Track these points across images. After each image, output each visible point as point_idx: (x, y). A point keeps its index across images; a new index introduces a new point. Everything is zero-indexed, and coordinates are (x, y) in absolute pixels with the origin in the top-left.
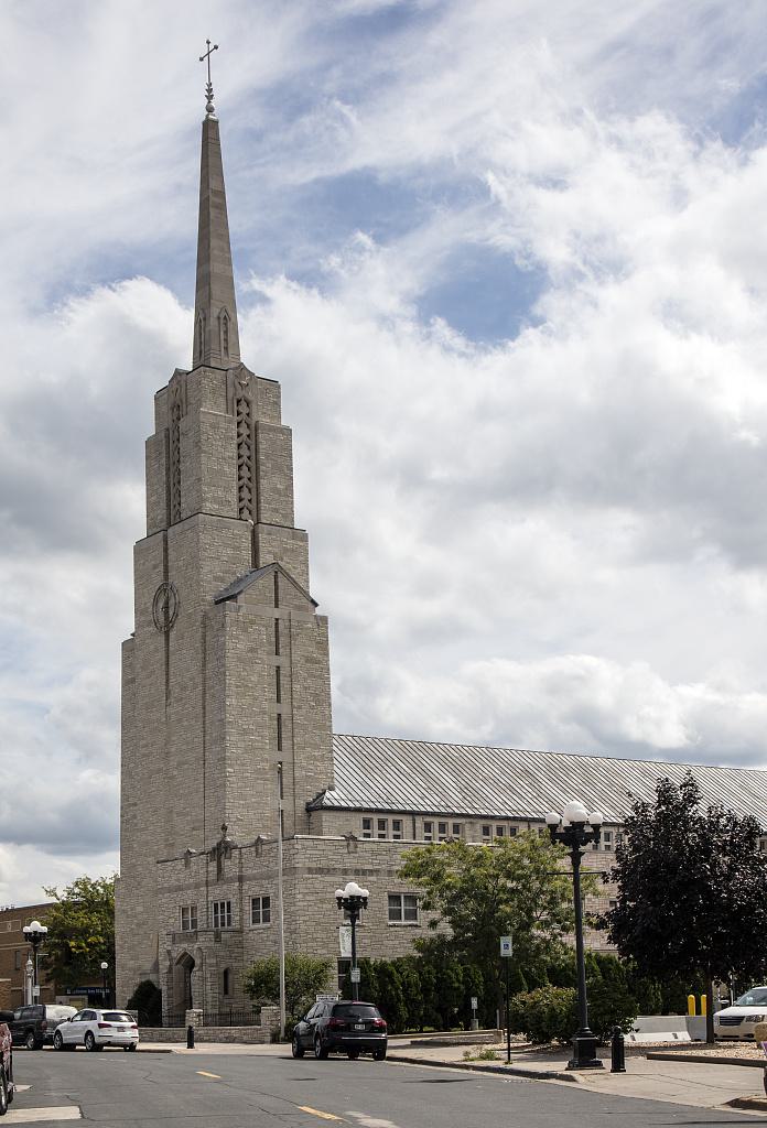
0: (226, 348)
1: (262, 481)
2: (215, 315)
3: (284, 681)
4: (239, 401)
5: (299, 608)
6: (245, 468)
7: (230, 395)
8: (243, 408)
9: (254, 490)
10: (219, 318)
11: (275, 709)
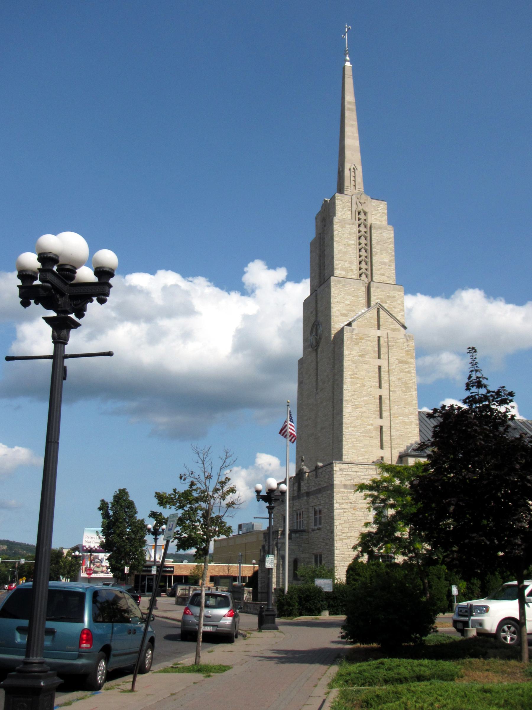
0: (355, 185)
1: (373, 257)
2: (348, 168)
3: (384, 375)
4: (359, 213)
5: (394, 330)
6: (363, 250)
7: (354, 209)
8: (362, 216)
9: (369, 263)
10: (350, 169)
11: (378, 392)
